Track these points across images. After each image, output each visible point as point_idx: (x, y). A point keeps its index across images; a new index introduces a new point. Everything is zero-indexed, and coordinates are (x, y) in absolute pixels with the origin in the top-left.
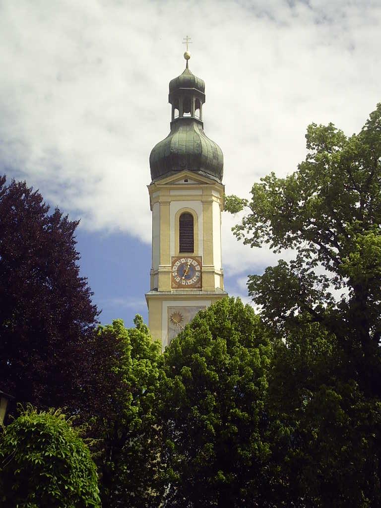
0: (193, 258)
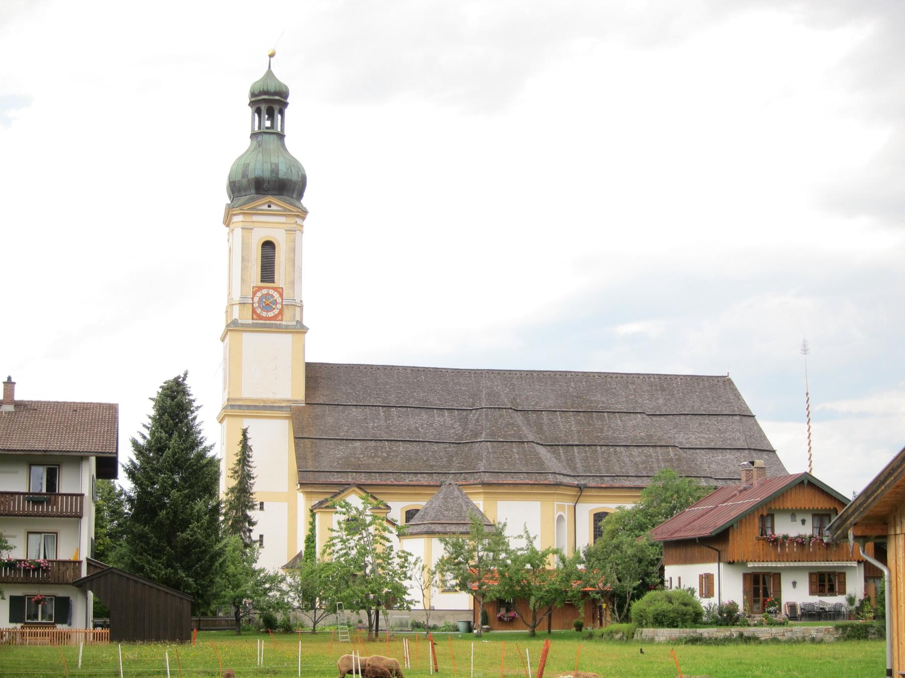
0: (275, 289)
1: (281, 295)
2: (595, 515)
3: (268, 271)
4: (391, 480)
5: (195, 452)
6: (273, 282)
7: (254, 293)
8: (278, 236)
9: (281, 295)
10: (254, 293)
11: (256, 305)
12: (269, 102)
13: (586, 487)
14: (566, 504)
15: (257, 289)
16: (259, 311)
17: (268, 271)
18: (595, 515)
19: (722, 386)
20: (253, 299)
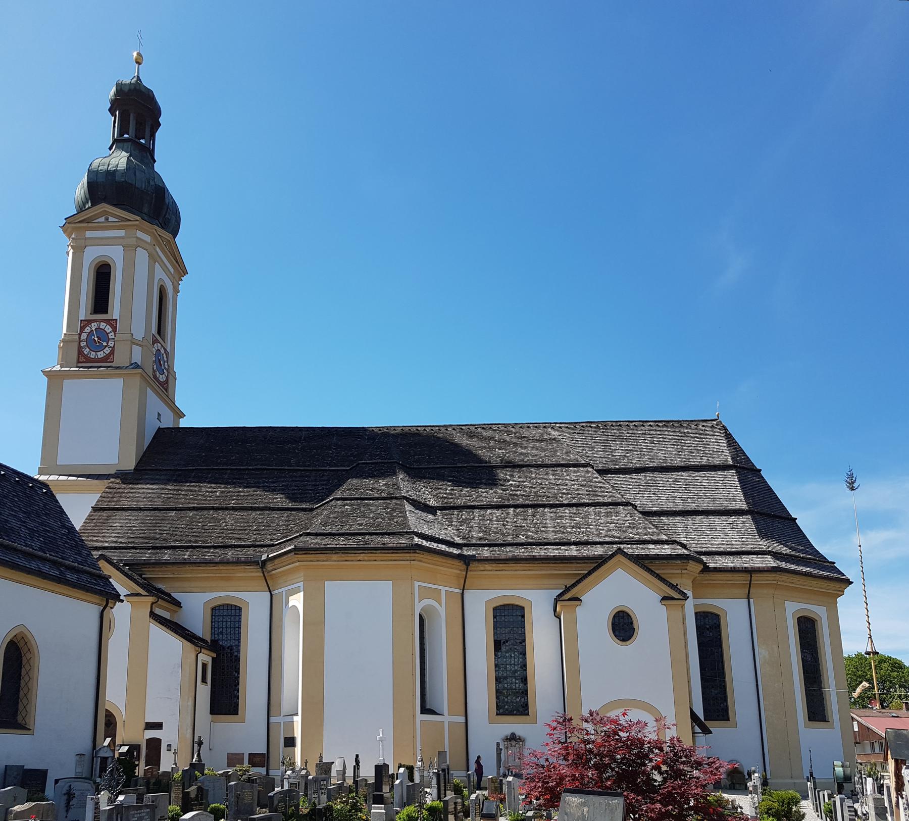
0: (108, 322)
1: (114, 329)
2: (495, 609)
3: (101, 302)
4: (209, 555)
5: (334, 773)
6: (107, 313)
7: (82, 329)
8: (818, 611)
9: (114, 329)
10: (82, 329)
11: (83, 344)
12: (136, 112)
13: (473, 558)
14: (443, 589)
15: (86, 323)
16: (86, 351)
17: (101, 302)
18: (495, 609)
19: (160, 125)
20: (80, 335)
